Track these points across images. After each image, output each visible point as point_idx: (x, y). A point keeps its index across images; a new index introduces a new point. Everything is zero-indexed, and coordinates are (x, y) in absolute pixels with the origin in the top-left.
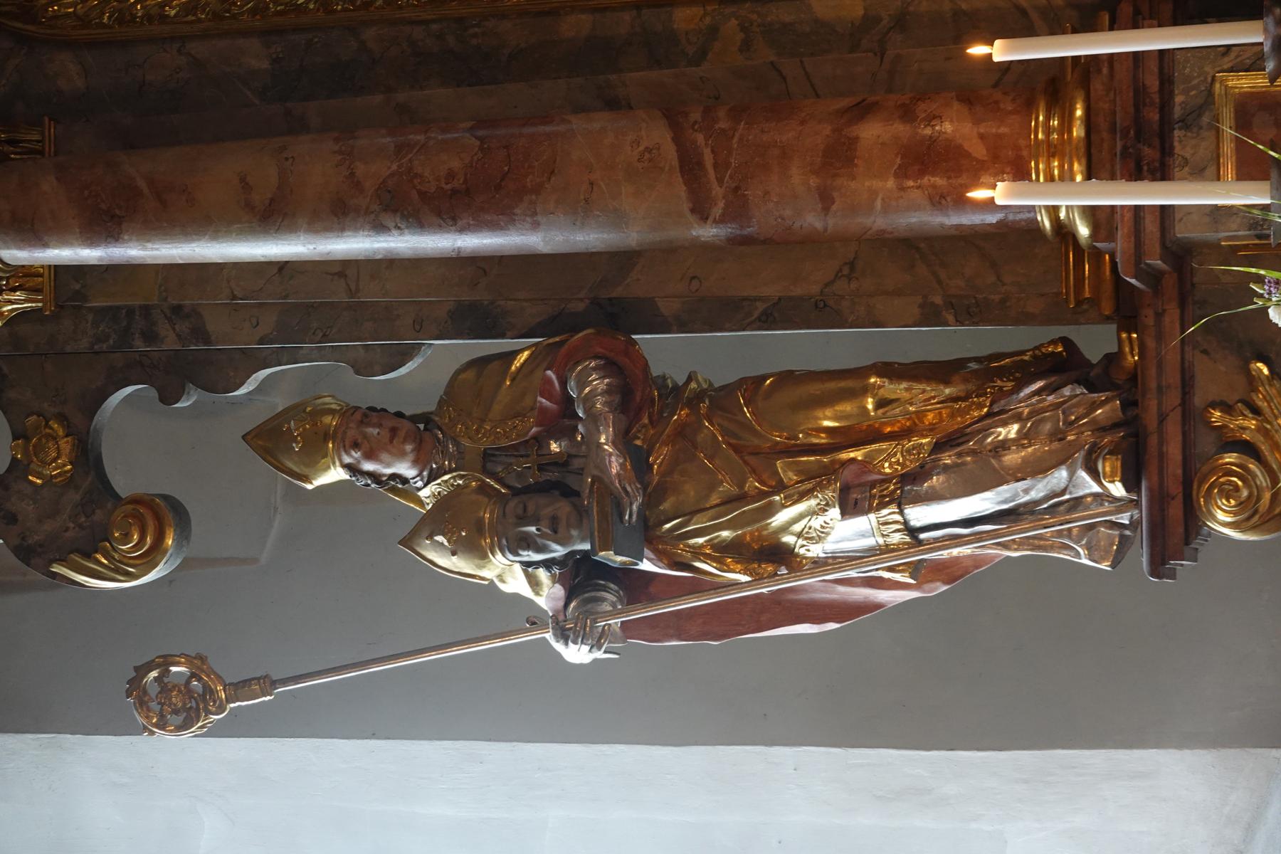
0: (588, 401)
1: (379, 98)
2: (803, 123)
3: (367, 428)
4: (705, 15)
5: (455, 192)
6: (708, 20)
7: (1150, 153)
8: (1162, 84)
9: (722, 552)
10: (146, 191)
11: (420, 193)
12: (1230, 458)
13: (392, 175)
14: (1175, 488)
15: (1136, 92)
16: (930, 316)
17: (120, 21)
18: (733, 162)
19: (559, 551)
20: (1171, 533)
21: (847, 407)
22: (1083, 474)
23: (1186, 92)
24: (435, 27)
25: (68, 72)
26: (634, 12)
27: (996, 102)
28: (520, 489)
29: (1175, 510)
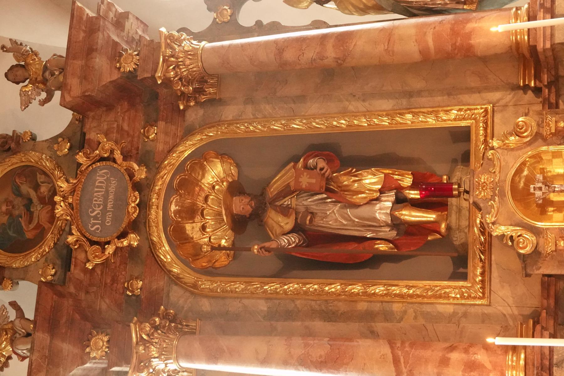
1: (299, 323)
2: (433, 351)
5: (321, 362)
6: (404, 308)
8: (550, 351)
10: (226, 350)
11: (311, 361)
13: (302, 354)
15: (541, 354)
17: (223, 291)
18: (410, 362)
23: (558, 355)
24: (318, 302)
25: (206, 305)
27: (495, 351)
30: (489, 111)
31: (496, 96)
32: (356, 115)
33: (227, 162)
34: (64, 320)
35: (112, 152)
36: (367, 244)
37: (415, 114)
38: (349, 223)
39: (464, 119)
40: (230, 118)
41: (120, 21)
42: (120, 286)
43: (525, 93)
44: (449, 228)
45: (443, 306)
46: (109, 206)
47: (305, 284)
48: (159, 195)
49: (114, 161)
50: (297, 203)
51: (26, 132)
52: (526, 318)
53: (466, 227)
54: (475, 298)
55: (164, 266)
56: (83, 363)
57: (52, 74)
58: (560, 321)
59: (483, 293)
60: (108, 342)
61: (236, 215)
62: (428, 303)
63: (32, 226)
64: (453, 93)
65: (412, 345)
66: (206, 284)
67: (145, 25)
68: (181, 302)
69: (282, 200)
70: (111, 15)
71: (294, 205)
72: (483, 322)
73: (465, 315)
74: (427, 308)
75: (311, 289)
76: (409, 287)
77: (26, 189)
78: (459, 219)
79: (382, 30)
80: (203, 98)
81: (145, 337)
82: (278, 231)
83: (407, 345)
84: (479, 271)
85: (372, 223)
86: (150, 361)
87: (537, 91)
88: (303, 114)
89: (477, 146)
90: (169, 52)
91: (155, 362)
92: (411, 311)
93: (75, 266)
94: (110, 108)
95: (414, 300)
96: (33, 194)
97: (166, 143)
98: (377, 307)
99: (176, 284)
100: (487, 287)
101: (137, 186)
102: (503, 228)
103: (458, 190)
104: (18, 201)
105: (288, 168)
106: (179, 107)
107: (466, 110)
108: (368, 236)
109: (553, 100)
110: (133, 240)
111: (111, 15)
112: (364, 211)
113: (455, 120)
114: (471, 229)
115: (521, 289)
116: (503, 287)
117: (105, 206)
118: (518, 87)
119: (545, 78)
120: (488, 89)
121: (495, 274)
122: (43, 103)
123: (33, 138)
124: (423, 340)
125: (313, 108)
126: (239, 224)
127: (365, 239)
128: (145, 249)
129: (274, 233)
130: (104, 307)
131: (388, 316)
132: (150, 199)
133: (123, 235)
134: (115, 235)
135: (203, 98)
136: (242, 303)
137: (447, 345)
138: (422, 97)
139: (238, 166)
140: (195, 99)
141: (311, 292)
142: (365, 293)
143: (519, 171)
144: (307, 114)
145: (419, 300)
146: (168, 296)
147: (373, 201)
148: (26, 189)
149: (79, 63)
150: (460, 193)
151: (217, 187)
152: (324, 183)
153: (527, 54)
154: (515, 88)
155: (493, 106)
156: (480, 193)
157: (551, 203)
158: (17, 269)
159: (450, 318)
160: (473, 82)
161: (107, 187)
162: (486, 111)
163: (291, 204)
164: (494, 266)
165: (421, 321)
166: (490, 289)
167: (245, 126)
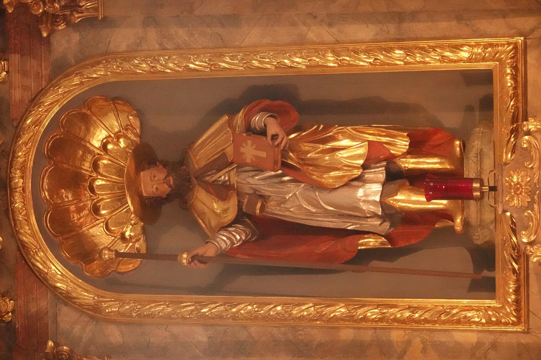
4: (405, 335)
6: (406, 337)
17: (138, 316)
24: (282, 329)
26: (373, 331)
30: (519, 47)
32: (320, 47)
33: (123, 111)
36: (348, 240)
37: (409, 51)
38: (319, 210)
39: (484, 59)
40: (123, 47)
44: (466, 224)
45: (462, 334)
47: (261, 305)
48: (23, 169)
50: (239, 180)
53: (491, 222)
54: (506, 324)
55: (46, 280)
59: (518, 318)
61: (149, 198)
62: (440, 330)
66: (111, 307)
69: (215, 173)
73: (494, 346)
74: (441, 338)
75: (272, 313)
80: (77, 18)
84: (512, 287)
85: (353, 212)
88: (237, 43)
92: (417, 341)
95: (421, 326)
97: (25, 88)
98: (368, 336)
99: (66, 304)
103: (480, 190)
106: (41, 34)
107: (485, 47)
108: (349, 228)
112: (342, 196)
113: (469, 60)
114: (498, 226)
125: (253, 35)
126: (150, 210)
128: (12, 249)
129: (207, 223)
132: (11, 179)
136: (170, 331)
138: (419, 21)
139: (140, 115)
141: (272, 316)
142: (350, 318)
144: (243, 45)
147: (352, 176)
150: (482, 193)
151: (110, 147)
155: (525, 39)
156: (512, 198)
163: (229, 180)
164: (532, 277)
166: (528, 310)
167: (147, 64)
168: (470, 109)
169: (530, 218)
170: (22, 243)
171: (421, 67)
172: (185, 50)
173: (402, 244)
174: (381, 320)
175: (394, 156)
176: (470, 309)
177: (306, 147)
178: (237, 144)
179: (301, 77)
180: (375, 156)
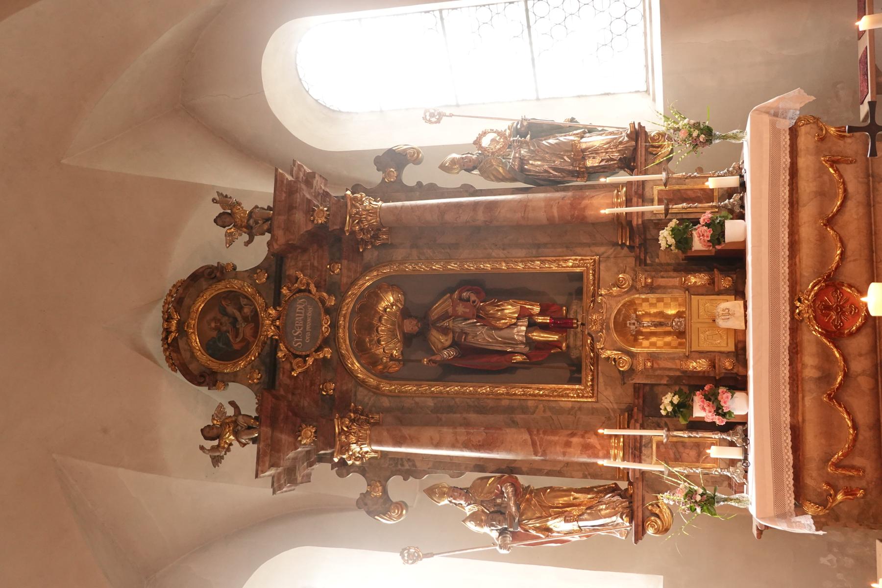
0: (508, 493)
3: (454, 492)
7: (637, 453)
9: (536, 529)
12: (653, 518)
14: (641, 523)
16: (585, 477)
19: (500, 527)
20: (640, 533)
21: (565, 499)
22: (619, 518)
25: (386, 402)
28: (494, 513)
29: (640, 528)
31: (602, 249)
32: (498, 260)
34: (282, 416)
35: (308, 284)
37: (542, 262)
39: (579, 266)
40: (400, 258)
41: (309, 180)
42: (316, 388)
43: (622, 249)
44: (568, 347)
46: (308, 327)
47: (462, 387)
49: (310, 292)
51: (228, 264)
52: (623, 411)
54: (587, 397)
56: (296, 448)
57: (256, 223)
58: (646, 413)
60: (315, 432)
63: (238, 340)
64: (570, 248)
65: (545, 433)
66: (386, 387)
67: (326, 180)
68: (366, 399)
70: (301, 175)
71: (451, 326)
72: (593, 414)
73: (580, 409)
74: (553, 405)
76: (540, 390)
77: (231, 310)
78: (575, 340)
79: (520, 201)
80: (378, 243)
81: (345, 429)
82: (440, 346)
83: (541, 432)
86: (349, 447)
87: (631, 248)
89: (588, 287)
90: (354, 211)
91: (353, 446)
93: (284, 373)
94: (305, 250)
96: (237, 314)
97: (349, 277)
98: (516, 404)
99: (362, 386)
100: (596, 388)
101: (328, 311)
102: (609, 352)
104: (225, 319)
105: (445, 298)
109: (642, 257)
110: (327, 353)
111: (301, 175)
112: (504, 333)
113: (572, 267)
115: (619, 391)
116: (606, 389)
117: (305, 328)
118: (617, 244)
119: (637, 241)
120: (595, 244)
121: (601, 380)
122: (247, 244)
123: (234, 268)
124: (553, 429)
126: (408, 340)
127: (504, 353)
130: (306, 404)
131: (524, 410)
132: (339, 321)
133: (319, 349)
134: (313, 349)
135: (378, 243)
137: (570, 432)
139: (404, 294)
140: (372, 243)
142: (508, 394)
143: (619, 311)
145: (547, 398)
146: (355, 395)
148: (231, 310)
149: (282, 218)
152: (475, 311)
153: (624, 223)
154: (615, 244)
157: (641, 333)
158: (227, 373)
159: (570, 411)
160: (585, 239)
161: (306, 312)
162: (595, 260)
164: (600, 374)
165: (548, 414)
168: (570, 294)
169: (601, 337)
170: (342, 355)
171: (548, 270)
172: (429, 260)
173: (534, 360)
174: (523, 395)
175: (533, 315)
176: (568, 389)
177: (488, 308)
178: (454, 307)
179: (486, 274)
180: (523, 314)
